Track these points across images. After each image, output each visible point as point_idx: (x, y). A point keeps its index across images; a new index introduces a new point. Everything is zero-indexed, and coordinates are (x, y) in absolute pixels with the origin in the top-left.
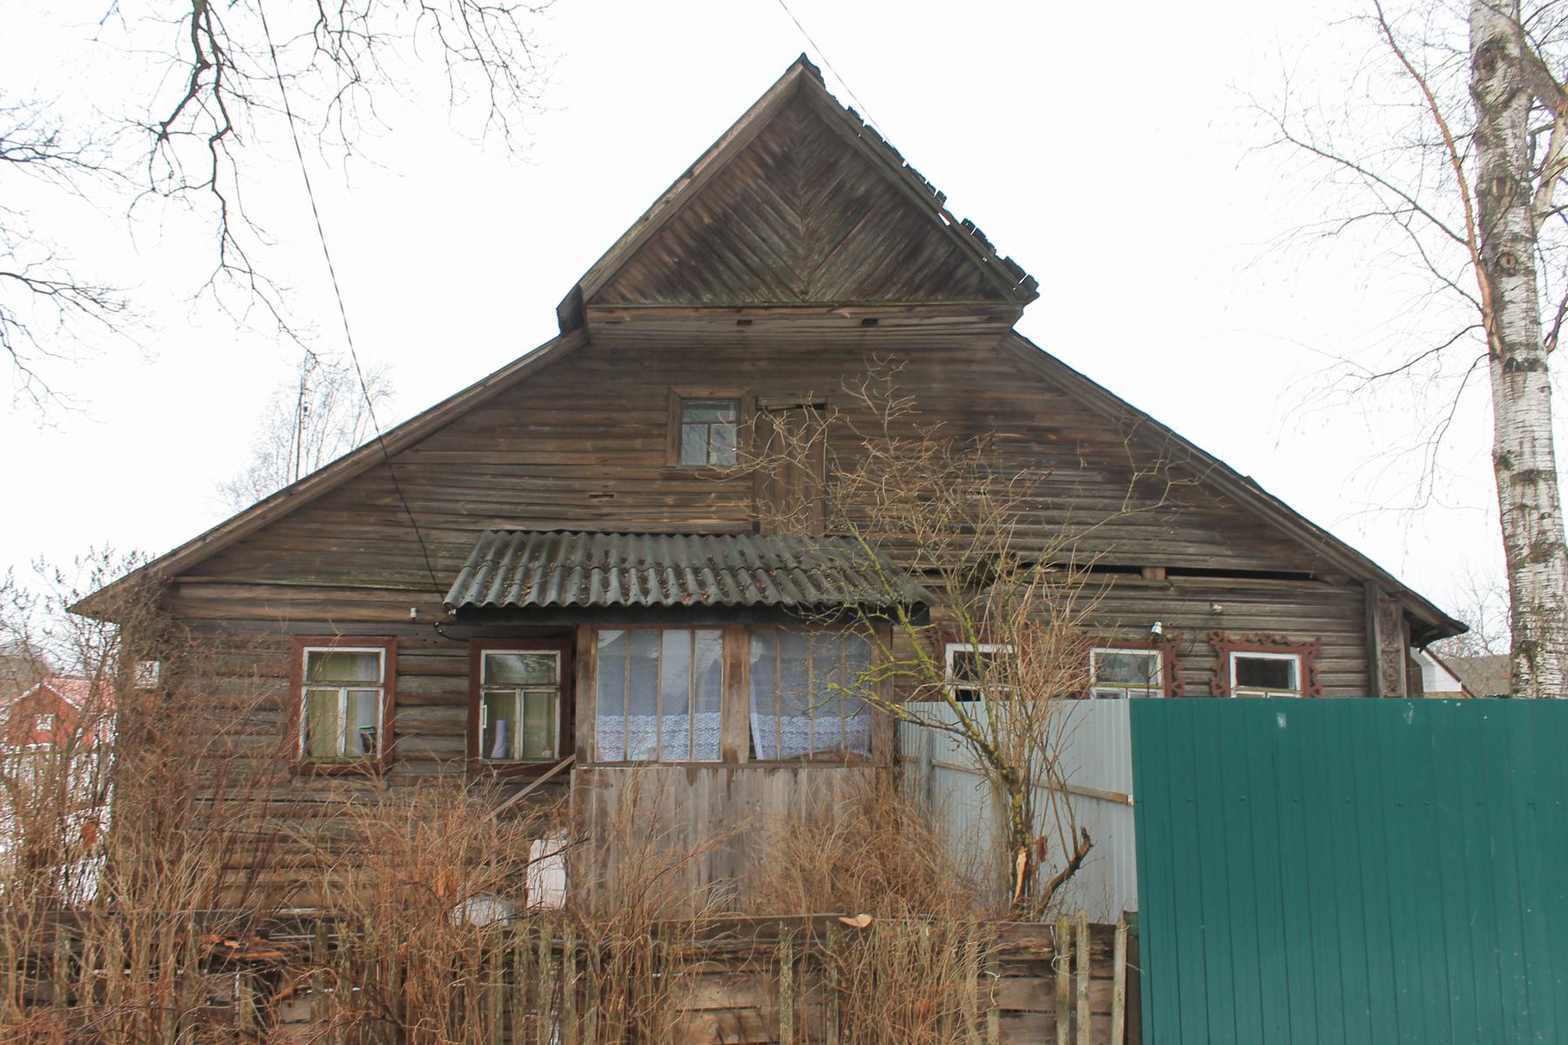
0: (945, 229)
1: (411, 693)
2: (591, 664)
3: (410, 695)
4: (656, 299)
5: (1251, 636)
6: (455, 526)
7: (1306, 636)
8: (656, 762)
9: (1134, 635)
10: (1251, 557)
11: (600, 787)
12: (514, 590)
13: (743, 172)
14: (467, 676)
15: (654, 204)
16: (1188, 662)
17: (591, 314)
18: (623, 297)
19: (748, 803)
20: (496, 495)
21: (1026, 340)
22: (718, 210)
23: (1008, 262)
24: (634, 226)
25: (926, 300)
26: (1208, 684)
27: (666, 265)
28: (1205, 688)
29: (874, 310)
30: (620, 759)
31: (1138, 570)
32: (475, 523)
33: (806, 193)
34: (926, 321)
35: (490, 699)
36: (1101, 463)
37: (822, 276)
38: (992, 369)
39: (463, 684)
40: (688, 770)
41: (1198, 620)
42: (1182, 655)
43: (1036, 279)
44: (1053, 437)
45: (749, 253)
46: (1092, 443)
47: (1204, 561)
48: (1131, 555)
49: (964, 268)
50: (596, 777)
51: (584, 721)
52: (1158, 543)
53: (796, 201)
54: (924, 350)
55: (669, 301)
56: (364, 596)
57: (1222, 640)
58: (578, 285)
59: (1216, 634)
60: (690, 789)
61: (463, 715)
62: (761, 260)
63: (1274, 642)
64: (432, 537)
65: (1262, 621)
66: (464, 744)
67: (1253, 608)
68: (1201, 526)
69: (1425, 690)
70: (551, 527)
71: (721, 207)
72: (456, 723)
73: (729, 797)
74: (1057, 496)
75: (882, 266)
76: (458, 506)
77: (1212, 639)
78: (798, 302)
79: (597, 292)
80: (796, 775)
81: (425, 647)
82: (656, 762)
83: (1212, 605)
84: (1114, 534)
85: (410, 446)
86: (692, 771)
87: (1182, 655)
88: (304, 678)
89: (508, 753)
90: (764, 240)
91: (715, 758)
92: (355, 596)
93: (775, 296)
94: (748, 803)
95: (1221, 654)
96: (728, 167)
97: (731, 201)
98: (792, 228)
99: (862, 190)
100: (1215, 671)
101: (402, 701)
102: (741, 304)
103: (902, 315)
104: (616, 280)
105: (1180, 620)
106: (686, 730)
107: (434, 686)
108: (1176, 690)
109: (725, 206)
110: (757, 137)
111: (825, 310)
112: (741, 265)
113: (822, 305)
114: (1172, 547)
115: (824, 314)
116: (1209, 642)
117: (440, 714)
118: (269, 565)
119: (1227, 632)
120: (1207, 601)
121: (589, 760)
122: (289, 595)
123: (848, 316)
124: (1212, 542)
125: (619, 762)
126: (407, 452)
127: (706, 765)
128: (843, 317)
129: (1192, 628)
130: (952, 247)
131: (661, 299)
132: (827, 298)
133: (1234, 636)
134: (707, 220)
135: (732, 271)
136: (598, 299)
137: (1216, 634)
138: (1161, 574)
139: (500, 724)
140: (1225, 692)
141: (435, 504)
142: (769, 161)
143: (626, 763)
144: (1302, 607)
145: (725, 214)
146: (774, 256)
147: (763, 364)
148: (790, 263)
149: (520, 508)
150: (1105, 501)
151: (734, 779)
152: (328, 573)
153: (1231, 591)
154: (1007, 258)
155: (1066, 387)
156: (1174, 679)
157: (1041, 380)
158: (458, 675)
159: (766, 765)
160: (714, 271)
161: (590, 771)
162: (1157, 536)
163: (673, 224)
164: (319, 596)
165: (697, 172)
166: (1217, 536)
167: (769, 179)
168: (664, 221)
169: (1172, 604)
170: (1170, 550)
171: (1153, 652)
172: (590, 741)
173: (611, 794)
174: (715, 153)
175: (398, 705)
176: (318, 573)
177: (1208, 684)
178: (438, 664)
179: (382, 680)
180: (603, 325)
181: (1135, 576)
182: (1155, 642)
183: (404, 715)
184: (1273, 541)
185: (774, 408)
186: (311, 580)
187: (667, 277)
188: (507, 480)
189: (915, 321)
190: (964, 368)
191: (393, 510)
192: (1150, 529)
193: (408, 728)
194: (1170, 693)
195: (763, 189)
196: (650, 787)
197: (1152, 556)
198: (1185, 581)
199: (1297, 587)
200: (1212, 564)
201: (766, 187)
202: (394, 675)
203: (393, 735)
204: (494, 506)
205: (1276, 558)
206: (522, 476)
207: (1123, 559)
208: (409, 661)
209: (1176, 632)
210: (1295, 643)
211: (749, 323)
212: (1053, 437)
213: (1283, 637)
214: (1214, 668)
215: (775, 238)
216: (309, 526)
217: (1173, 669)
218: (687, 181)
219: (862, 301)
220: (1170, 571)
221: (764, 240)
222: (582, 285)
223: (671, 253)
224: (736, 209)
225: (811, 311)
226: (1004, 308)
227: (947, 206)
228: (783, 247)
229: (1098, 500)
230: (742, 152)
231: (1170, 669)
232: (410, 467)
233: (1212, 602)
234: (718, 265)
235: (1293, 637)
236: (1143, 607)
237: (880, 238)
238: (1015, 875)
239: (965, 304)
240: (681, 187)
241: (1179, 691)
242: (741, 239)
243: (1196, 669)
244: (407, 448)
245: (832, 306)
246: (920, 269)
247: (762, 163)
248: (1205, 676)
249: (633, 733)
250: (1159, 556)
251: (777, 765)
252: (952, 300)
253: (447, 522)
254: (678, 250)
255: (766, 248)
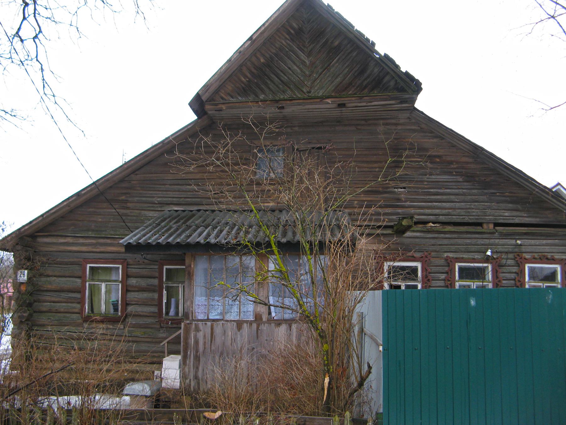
0: (377, 59)
1: (133, 285)
2: (191, 272)
3: (133, 286)
4: (238, 98)
5: (536, 256)
6: (152, 209)
7: (563, 255)
8: (223, 320)
9: (477, 256)
10: (536, 217)
11: (195, 331)
12: (172, 238)
13: (279, 37)
14: (157, 278)
15: (234, 54)
16: (505, 269)
17: (208, 107)
18: (222, 98)
19: (267, 340)
20: (171, 194)
21: (422, 113)
22: (268, 56)
23: (407, 74)
24: (225, 64)
25: (368, 94)
26: (514, 280)
27: (242, 82)
28: (513, 282)
29: (343, 99)
30: (206, 318)
31: (480, 224)
32: (161, 207)
33: (310, 45)
34: (369, 104)
35: (168, 289)
36: (461, 172)
37: (318, 84)
38: (409, 127)
39: (156, 282)
40: (237, 324)
41: (510, 248)
42: (501, 266)
43: (420, 81)
44: (438, 160)
45: (282, 75)
46: (457, 162)
47: (512, 219)
48: (477, 217)
49: (387, 78)
50: (193, 326)
51: (188, 300)
52: (490, 211)
53: (305, 49)
54: (375, 119)
55: (244, 99)
56: (112, 241)
57: (521, 258)
58: (198, 93)
59: (518, 255)
60: (238, 333)
61: (156, 296)
62: (288, 78)
63: (547, 259)
64: (142, 214)
65: (541, 249)
66: (155, 309)
67: (537, 242)
68: (511, 202)
69: (157, 295)
70: (195, 208)
71: (269, 54)
72: (153, 299)
73: (257, 337)
74: (440, 189)
75: (347, 78)
76: (154, 199)
77: (516, 258)
78: (306, 96)
79: (210, 97)
80: (290, 327)
81: (139, 265)
82: (223, 320)
83: (516, 241)
84: (468, 207)
85: (134, 172)
86: (239, 324)
87: (501, 266)
88: (457, 278)
89: (177, 313)
90: (290, 68)
91: (251, 318)
92: (109, 241)
93: (295, 95)
94: (267, 340)
95: (521, 265)
96: (273, 35)
97: (274, 51)
98: (303, 63)
99: (337, 43)
100: (518, 273)
101: (129, 289)
102: (278, 99)
103: (357, 101)
104: (219, 91)
105: (500, 248)
106: (238, 305)
107: (143, 283)
108: (498, 283)
109: (271, 54)
110: (286, 21)
111: (319, 100)
112: (278, 80)
113: (318, 98)
114: (498, 213)
115: (319, 102)
116: (515, 259)
117: (145, 295)
118: (73, 227)
119: (524, 254)
120: (514, 239)
121: (191, 318)
122: (81, 241)
123: (331, 103)
124: (517, 210)
125: (205, 319)
126: (132, 175)
127: (247, 322)
128: (329, 103)
129: (506, 253)
130: (381, 68)
131: (240, 98)
132: (320, 94)
133: (528, 256)
134: (262, 60)
135: (274, 84)
136: (211, 99)
137: (518, 255)
138: (491, 226)
139: (173, 301)
140: (523, 284)
141: (144, 199)
142: (292, 32)
143: (208, 320)
144: (561, 241)
145: (271, 57)
146: (295, 76)
147: (296, 129)
148: (302, 78)
149: (182, 199)
150: (464, 191)
151: (260, 328)
152: (97, 231)
153: (526, 234)
154: (406, 72)
155: (444, 135)
156: (497, 277)
157: (432, 132)
158: (154, 278)
159: (276, 322)
160: (266, 84)
161: (191, 323)
162: (489, 208)
163: (246, 63)
164: (94, 241)
165: (254, 37)
166: (519, 207)
167: (292, 40)
168: (242, 62)
169: (497, 241)
170: (496, 214)
171: (485, 265)
172: (191, 309)
173: (200, 335)
174: (263, 28)
175: (127, 291)
176: (93, 231)
177: (514, 280)
178: (144, 272)
179: (120, 280)
180: (214, 112)
181: (479, 227)
182: (487, 260)
183: (131, 296)
184: (547, 209)
185: (302, 149)
186: (90, 234)
187: (243, 88)
188: (176, 187)
189: (364, 104)
190: (394, 127)
191: (126, 202)
192: (486, 204)
193: (132, 301)
194: (495, 285)
195: (289, 45)
196: (218, 330)
197: (487, 217)
198: (503, 230)
199: (559, 231)
200: (517, 221)
201: (291, 43)
202: (125, 277)
203: (126, 304)
204: (170, 199)
205: (550, 217)
206: (183, 185)
207: (472, 219)
208: (132, 271)
209: (499, 255)
210: (558, 259)
211: (282, 108)
212: (438, 160)
213: (552, 256)
214: (517, 272)
215: (295, 67)
216: (91, 210)
217: (497, 273)
218: (249, 42)
219: (337, 95)
220: (496, 225)
221: (290, 68)
222: (200, 93)
223: (246, 76)
224: (276, 55)
225: (312, 101)
226: (407, 96)
227: (377, 48)
228: (299, 71)
229: (461, 190)
230: (279, 28)
231: (495, 273)
232: (133, 182)
233: (516, 239)
234: (267, 81)
235: (557, 256)
236: (482, 242)
237: (346, 65)
238: (323, 389)
239: (388, 95)
240: (246, 45)
241: (499, 283)
242: (278, 68)
243: (508, 274)
244: (131, 174)
245: (322, 98)
246: (366, 79)
247: (289, 33)
248: (513, 276)
249: (212, 305)
250: (490, 217)
251: (281, 322)
252: (381, 93)
253: (149, 207)
254: (249, 75)
255: (291, 72)
